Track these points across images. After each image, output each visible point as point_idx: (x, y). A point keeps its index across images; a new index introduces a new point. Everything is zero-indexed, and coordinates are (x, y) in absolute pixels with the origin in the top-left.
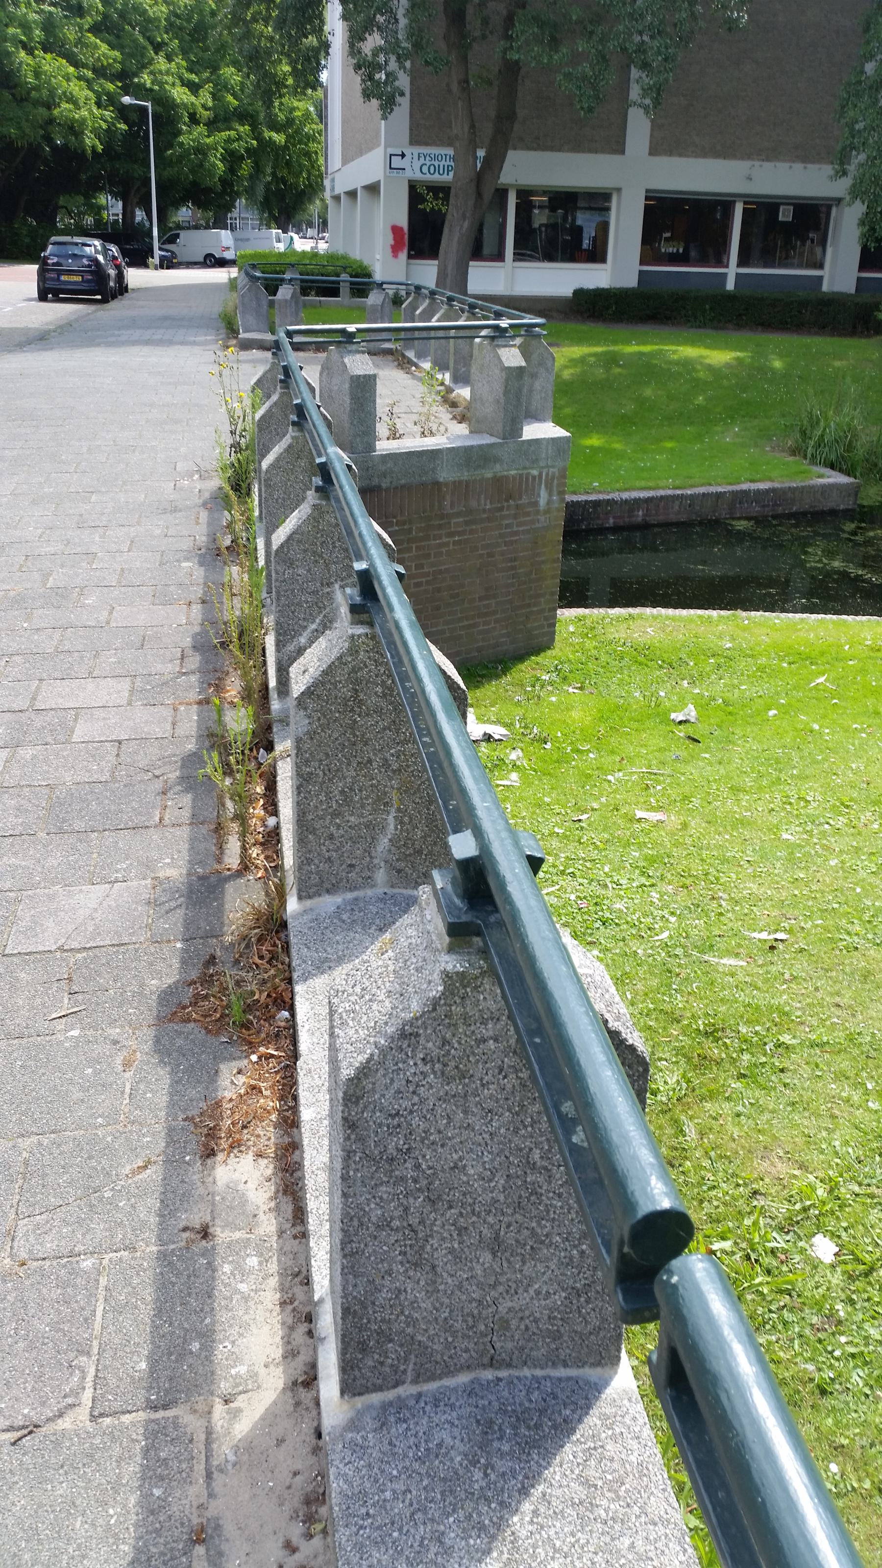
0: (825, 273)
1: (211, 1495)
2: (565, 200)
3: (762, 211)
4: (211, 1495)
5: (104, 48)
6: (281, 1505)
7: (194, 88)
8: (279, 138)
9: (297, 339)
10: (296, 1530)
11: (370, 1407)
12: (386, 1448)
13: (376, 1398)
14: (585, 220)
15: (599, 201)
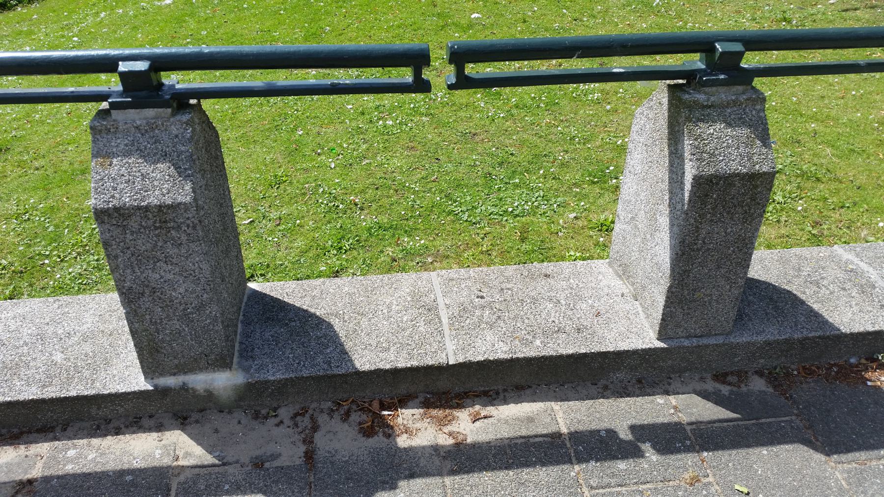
1: (237, 462)
4: (237, 462)
6: (254, 429)
9: (406, 75)
10: (272, 421)
11: (239, 363)
12: (265, 356)
13: (235, 360)
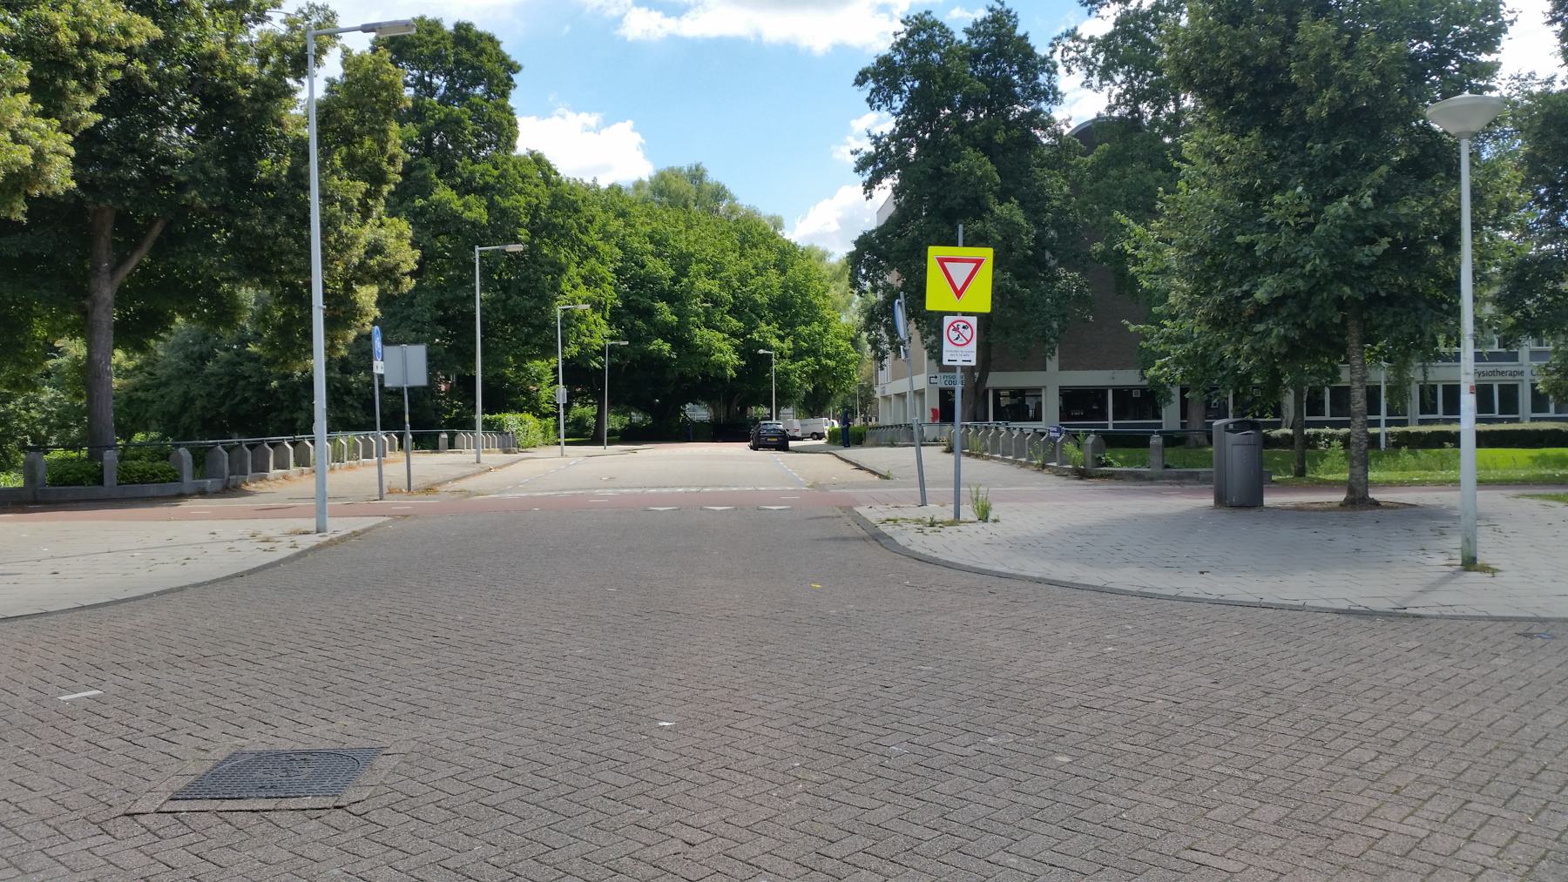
0: (1163, 421)
2: (1019, 393)
3: (1121, 394)
5: (734, 322)
7: (781, 338)
8: (832, 363)
14: (1030, 402)
15: (1037, 392)
